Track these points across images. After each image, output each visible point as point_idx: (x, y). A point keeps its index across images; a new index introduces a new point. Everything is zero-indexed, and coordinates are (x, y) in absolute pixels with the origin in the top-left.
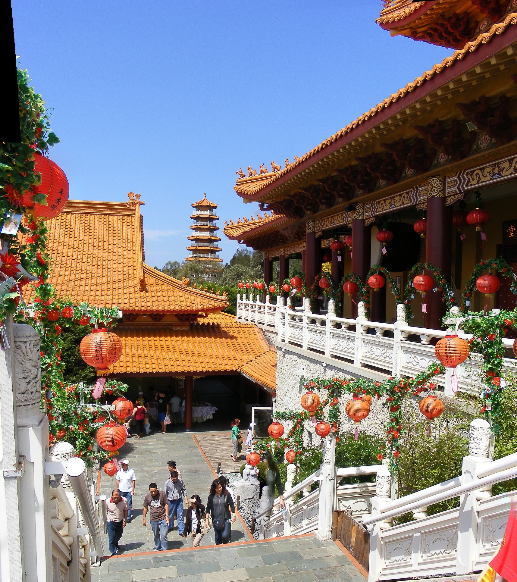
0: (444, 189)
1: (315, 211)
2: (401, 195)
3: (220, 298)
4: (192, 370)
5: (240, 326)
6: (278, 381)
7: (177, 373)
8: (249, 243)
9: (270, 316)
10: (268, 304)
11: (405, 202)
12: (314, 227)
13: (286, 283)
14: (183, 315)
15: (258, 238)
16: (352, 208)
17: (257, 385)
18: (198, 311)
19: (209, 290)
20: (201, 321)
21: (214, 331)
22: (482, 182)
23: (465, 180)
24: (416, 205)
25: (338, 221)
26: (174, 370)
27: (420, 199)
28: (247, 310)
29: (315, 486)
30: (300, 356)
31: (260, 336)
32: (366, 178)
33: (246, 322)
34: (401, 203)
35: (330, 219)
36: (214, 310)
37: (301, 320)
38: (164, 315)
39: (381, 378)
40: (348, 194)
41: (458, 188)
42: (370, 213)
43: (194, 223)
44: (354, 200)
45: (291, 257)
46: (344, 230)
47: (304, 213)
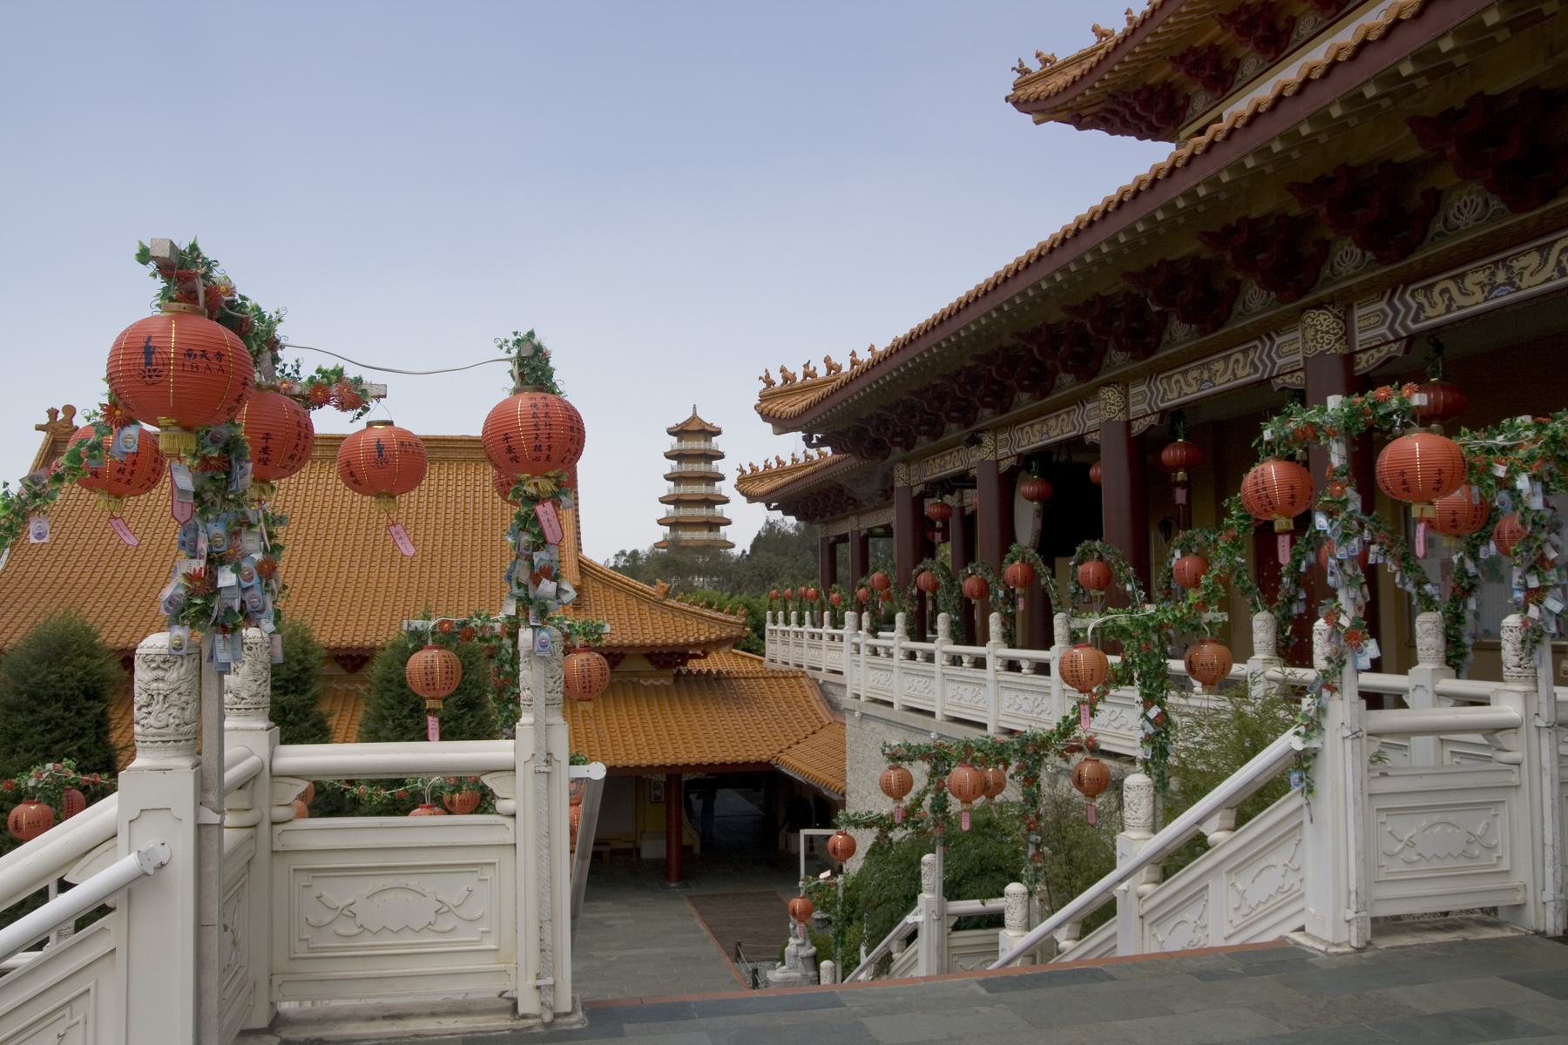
0: (1127, 406)
1: (908, 447)
2: (1227, 358)
3: (732, 618)
4: (681, 762)
5: (774, 676)
6: (850, 777)
7: (651, 767)
8: (787, 505)
9: (813, 651)
10: (827, 629)
11: (1240, 373)
12: (909, 478)
13: (862, 586)
14: (661, 654)
15: (800, 495)
16: (975, 441)
17: (809, 787)
18: (688, 645)
19: (709, 605)
20: (695, 665)
21: (715, 683)
22: (1460, 308)
23: (1408, 308)
24: (1269, 379)
25: (951, 464)
26: (644, 762)
27: (1280, 362)
28: (786, 643)
29: (912, 937)
30: (888, 722)
31: (813, 695)
32: (1078, 349)
33: (785, 668)
34: (1229, 375)
35: (1037, 427)
36: (718, 643)
37: (890, 655)
38: (623, 656)
39: (974, 734)
40: (966, 416)
41: (1391, 328)
42: (1384, 330)
43: (671, 466)
44: (975, 427)
45: (871, 533)
46: (963, 481)
47: (943, 425)
